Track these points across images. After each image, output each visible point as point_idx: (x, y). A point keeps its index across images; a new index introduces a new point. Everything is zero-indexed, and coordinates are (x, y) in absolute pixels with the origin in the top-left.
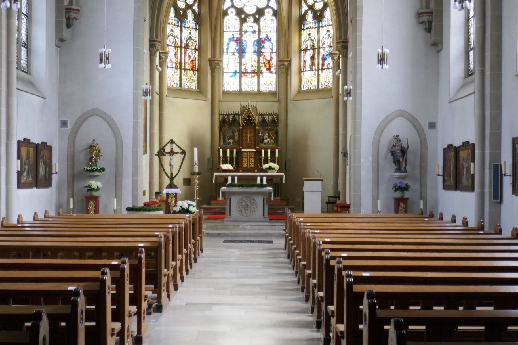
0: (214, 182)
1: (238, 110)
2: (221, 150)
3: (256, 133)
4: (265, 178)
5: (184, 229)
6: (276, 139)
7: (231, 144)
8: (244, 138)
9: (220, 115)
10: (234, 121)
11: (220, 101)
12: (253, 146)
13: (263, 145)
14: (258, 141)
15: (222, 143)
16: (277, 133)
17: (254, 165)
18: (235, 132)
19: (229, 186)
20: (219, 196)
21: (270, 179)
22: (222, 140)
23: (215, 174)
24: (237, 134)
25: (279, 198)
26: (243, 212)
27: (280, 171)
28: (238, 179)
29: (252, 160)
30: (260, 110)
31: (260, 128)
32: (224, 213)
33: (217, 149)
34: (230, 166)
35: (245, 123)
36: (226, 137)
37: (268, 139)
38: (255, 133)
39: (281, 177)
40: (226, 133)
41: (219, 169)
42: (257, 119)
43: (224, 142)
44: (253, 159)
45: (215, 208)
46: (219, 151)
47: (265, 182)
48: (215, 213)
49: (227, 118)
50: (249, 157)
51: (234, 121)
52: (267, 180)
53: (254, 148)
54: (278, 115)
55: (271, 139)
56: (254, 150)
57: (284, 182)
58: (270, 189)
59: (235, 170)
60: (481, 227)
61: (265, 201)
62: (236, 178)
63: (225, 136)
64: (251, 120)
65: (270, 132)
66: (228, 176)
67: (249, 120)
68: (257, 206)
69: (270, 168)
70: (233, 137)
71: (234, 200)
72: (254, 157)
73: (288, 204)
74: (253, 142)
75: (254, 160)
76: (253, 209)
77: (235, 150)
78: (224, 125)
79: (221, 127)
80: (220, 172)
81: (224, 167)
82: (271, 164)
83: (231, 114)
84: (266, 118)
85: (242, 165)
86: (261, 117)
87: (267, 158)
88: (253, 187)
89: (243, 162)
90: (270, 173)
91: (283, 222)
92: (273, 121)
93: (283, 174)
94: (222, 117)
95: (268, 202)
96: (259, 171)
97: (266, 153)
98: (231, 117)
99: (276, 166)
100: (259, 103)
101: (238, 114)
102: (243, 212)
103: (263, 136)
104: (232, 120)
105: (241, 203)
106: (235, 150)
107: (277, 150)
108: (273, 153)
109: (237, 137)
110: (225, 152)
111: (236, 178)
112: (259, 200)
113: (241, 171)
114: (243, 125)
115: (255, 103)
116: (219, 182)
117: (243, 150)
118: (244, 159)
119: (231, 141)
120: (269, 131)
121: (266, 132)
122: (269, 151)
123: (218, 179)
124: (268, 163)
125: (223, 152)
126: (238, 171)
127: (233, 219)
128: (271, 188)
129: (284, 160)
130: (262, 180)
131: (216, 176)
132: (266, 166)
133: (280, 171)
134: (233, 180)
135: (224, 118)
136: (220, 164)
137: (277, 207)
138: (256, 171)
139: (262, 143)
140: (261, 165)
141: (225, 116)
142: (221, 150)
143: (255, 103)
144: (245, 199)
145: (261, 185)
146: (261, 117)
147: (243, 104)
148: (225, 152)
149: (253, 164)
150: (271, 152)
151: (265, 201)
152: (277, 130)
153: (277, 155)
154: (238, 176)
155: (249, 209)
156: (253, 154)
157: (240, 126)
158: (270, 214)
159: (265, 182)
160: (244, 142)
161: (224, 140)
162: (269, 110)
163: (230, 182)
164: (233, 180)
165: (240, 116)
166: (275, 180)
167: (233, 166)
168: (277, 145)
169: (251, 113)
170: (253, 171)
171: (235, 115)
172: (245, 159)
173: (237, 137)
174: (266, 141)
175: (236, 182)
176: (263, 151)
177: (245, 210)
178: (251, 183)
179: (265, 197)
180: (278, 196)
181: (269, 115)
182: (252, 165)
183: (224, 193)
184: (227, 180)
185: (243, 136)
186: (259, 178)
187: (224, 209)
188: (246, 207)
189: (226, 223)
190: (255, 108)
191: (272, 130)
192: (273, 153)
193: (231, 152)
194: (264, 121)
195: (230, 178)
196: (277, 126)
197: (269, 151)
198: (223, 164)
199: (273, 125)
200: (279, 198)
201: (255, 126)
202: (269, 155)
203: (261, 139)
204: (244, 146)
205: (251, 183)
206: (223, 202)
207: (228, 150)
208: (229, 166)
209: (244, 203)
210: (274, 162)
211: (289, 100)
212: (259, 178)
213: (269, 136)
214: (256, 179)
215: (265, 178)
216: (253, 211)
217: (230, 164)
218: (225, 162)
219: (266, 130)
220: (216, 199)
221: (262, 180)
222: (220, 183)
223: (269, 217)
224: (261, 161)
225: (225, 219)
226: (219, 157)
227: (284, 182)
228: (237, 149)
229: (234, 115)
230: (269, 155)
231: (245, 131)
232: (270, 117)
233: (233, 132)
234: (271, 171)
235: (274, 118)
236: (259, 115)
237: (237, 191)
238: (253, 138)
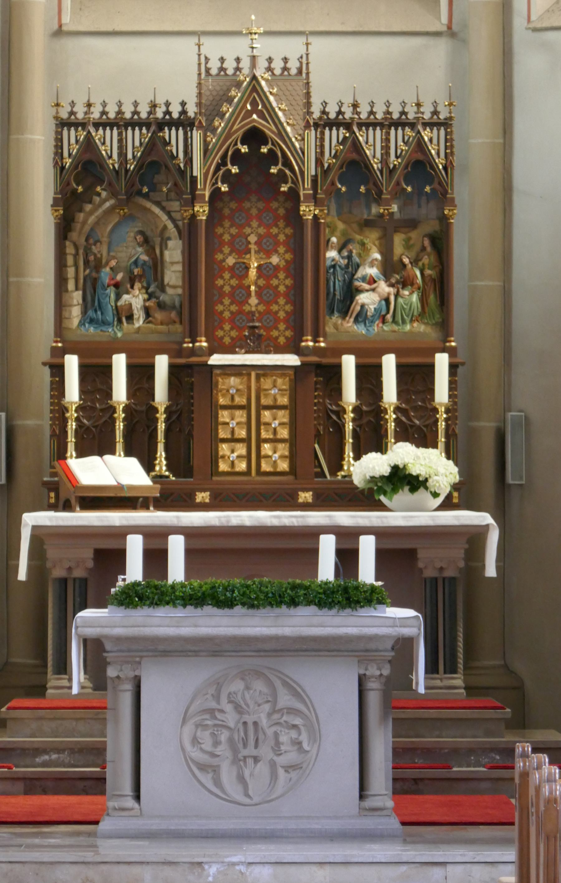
0: (22, 575)
1: (179, 91)
2: (72, 363)
3: (303, 242)
4: (367, 546)
5: (50, 669)
6: (439, 287)
7: (139, 321)
8: (227, 282)
9: (63, 124)
10: (155, 172)
11: (59, 32)
12: (282, 333)
13: (349, 324)
14: (316, 297)
15: (76, 312)
16: (440, 243)
17: (292, 458)
18: (164, 245)
19: (133, 597)
20: (63, 667)
21: (398, 552)
22: (77, 297)
23: (31, 519)
24: (174, 253)
25: (458, 681)
26: (228, 775)
27: (463, 496)
28: (189, 552)
29: (278, 422)
30: (330, 92)
31: (330, 216)
32: (97, 784)
33: (46, 356)
34: (133, 463)
35: (227, 177)
36: (105, 274)
37: (384, 288)
38: (297, 247)
39: (475, 538)
40: (102, 250)
41: (54, 487)
42: (309, 152)
43: (92, 303)
44: (283, 416)
45: (38, 751)
46: (58, 370)
47: (367, 572)
48: (33, 785)
49: (108, 143)
50: (253, 408)
51: (155, 172)
52: (382, 555)
53: (297, 351)
54: (446, 124)
55: (406, 282)
56: (292, 360)
57: (491, 571)
58: (401, 618)
59: (169, 498)
60: (296, 748)
61: (374, 700)
62: (176, 546)
63: (98, 266)
64: (272, 158)
65: (398, 240)
66: (122, 533)
67: (256, 162)
68: (315, 735)
69: (401, 479)
70: (150, 274)
71: (166, 694)
72: (293, 408)
73: (520, 722)
74: (282, 308)
75: (293, 425)
76: (291, 756)
77: (162, 363)
78: (87, 196)
79: (69, 205)
80: (67, 507)
81: (91, 471)
82: (404, 454)
83: (135, 123)
84: (372, 143)
85: (214, 459)
86: (333, 137)
87: (379, 412)
88: (293, 603)
89: (217, 441)
90: (403, 514)
91: (504, 842)
92: (419, 167)
93: (483, 518)
94: (72, 139)
95: (389, 705)
96: (323, 502)
97: (369, 376)
98: (135, 139)
99: (435, 465)
100: (317, 43)
101: (185, 123)
102: (228, 775)
103: (352, 267)
104: (141, 164)
105: (211, 712)
106: (162, 363)
107: (442, 361)
108: (417, 377)
109: (173, 276)
110: (96, 376)
111: (176, 546)
112: (333, 696)
113: (202, 497)
114: (216, 194)
115: (293, 48)
116: (58, 573)
117: (216, 359)
118: (224, 416)
119: (136, 299)
120: (387, 228)
121: (372, 238)
122: (389, 363)
123: (52, 553)
124: (381, 448)
125: (85, 372)
126: (186, 503)
127: (154, 825)
128: (410, 613)
129: (487, 425)
130: (347, 557)
131: (40, 536)
132: (375, 464)
133: (463, 496)
134: (156, 558)
135: (89, 144)
136: (62, 455)
137: (448, 739)
138: (306, 496)
139: (345, 313)
140: (337, 463)
141: (98, 135)
142: (72, 363)
143: (293, 48)
144: (237, 686)
145: (346, 595)
146: (333, 137)
147: (217, 50)
148: (96, 376)
149: (284, 449)
150: (401, 369)
151: (374, 700)
152: (445, 222)
153: (442, 393)
154: (190, 533)
155: (265, 752)
156: (283, 383)
157: (194, 199)
158: (402, 786)
159: (367, 572)
160: (226, 308)
161: (92, 289)
162: (384, 94)
163: (134, 570)
164: (156, 558)
165: (197, 136)
166: (431, 561)
167: (149, 466)
168: (445, 327)
169: (268, 113)
170: (288, 502)
171: (161, 125)
172: (231, 421)
173: (173, 276)
174: (368, 299)
175: (176, 570)
176: (349, 363)
177: (238, 761)
178: (273, 579)
179: (373, 671)
180: (452, 669)
181: (390, 123)
182: (276, 458)
183: (94, 649)
184: (111, 558)
185: (215, 269)
186: (328, 546)
187: (97, 753)
188: (246, 742)
189: (110, 849)
190: (299, 77)
191: (411, 224)
192: (417, 377)
193: (141, 375)
194: (354, 165)
195: (135, 546)
196: (443, 196)
197: (389, 363)
198: (81, 453)
199: (419, 191)
200: (458, 681)
201: (293, 196)
202: (390, 393)
203: (338, 284)
204: (226, 333)
205: (273, 579)
206: (93, 710)
207: (120, 363)
208: (120, 470)
209: (231, 718)
210: (424, 438)
211: (519, 23)
212: (328, 546)
213: (390, 268)
214: (314, 552)
215: (367, 546)
216: (287, 769)
217: (128, 453)
218: (96, 442)
219: (368, 224)
220: (40, 690)
221: (347, 557)
222: (63, 582)
223: (397, 810)
224: (340, 429)
225: (105, 825)
226: (60, 412)
227: (491, 571)
228: (175, 352)
229: (158, 124)
230: (390, 393)
231: (226, 232)
232: (397, 138)
233: (147, 241)
234: (403, 496)
235: (420, 145)
236: (326, 123)
237: (186, 631)
238: (283, 283)
